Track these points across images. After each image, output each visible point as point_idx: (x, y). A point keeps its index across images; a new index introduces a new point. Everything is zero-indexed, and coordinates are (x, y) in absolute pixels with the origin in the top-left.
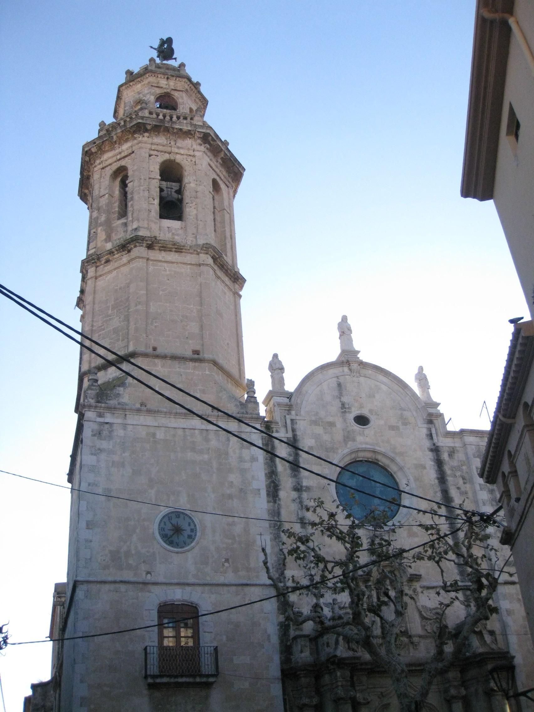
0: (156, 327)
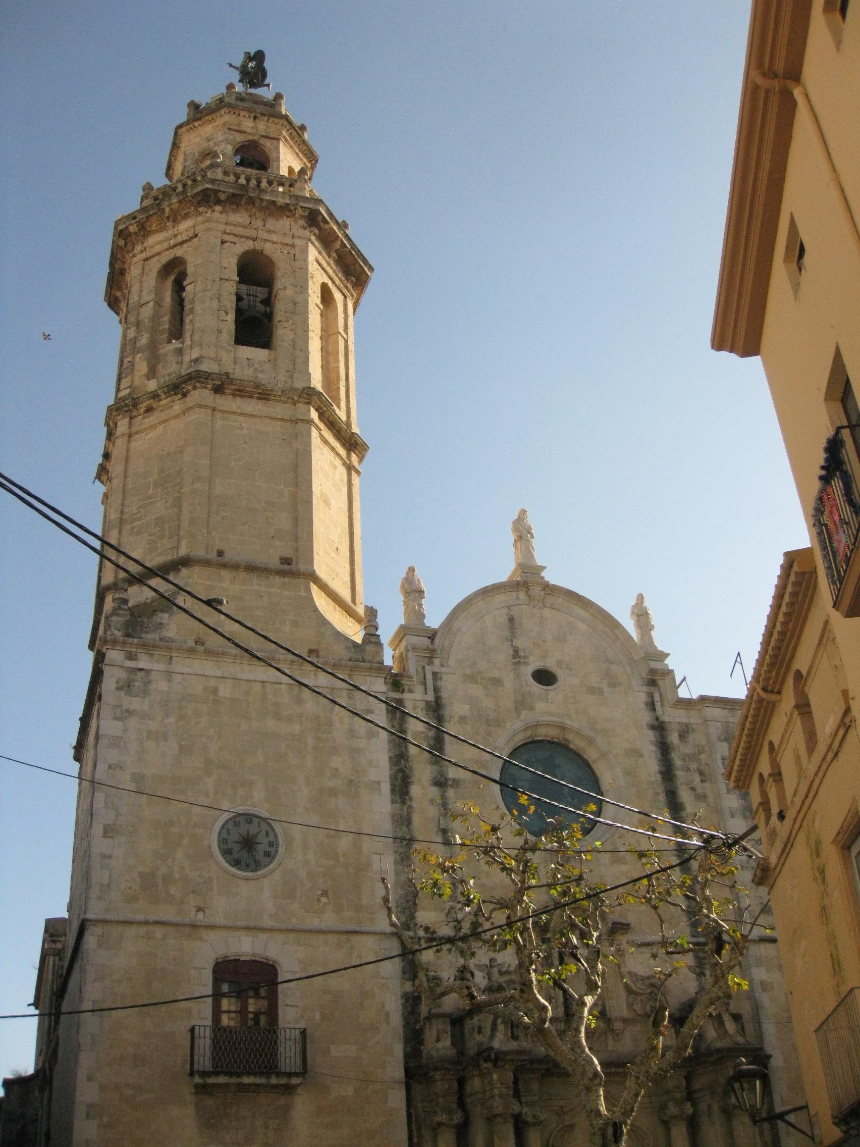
0: (223, 518)
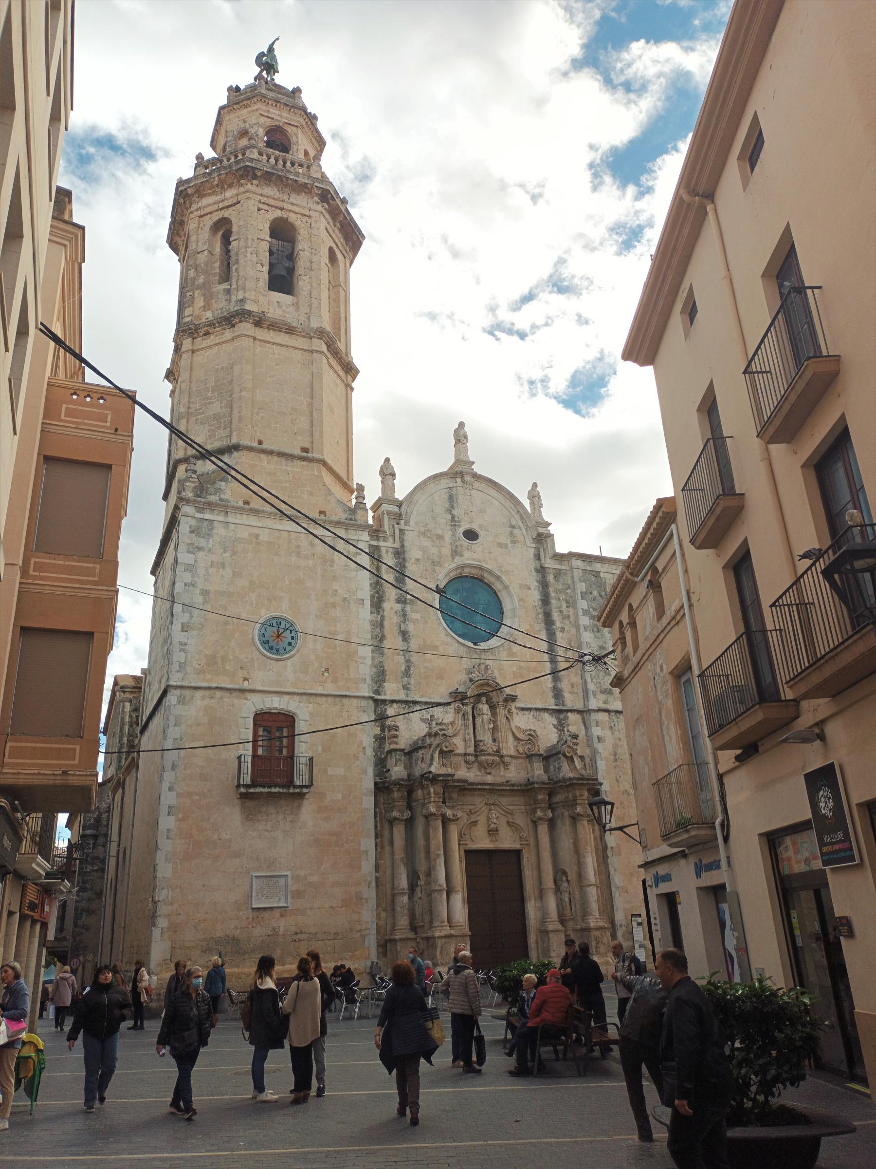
0: (262, 417)
